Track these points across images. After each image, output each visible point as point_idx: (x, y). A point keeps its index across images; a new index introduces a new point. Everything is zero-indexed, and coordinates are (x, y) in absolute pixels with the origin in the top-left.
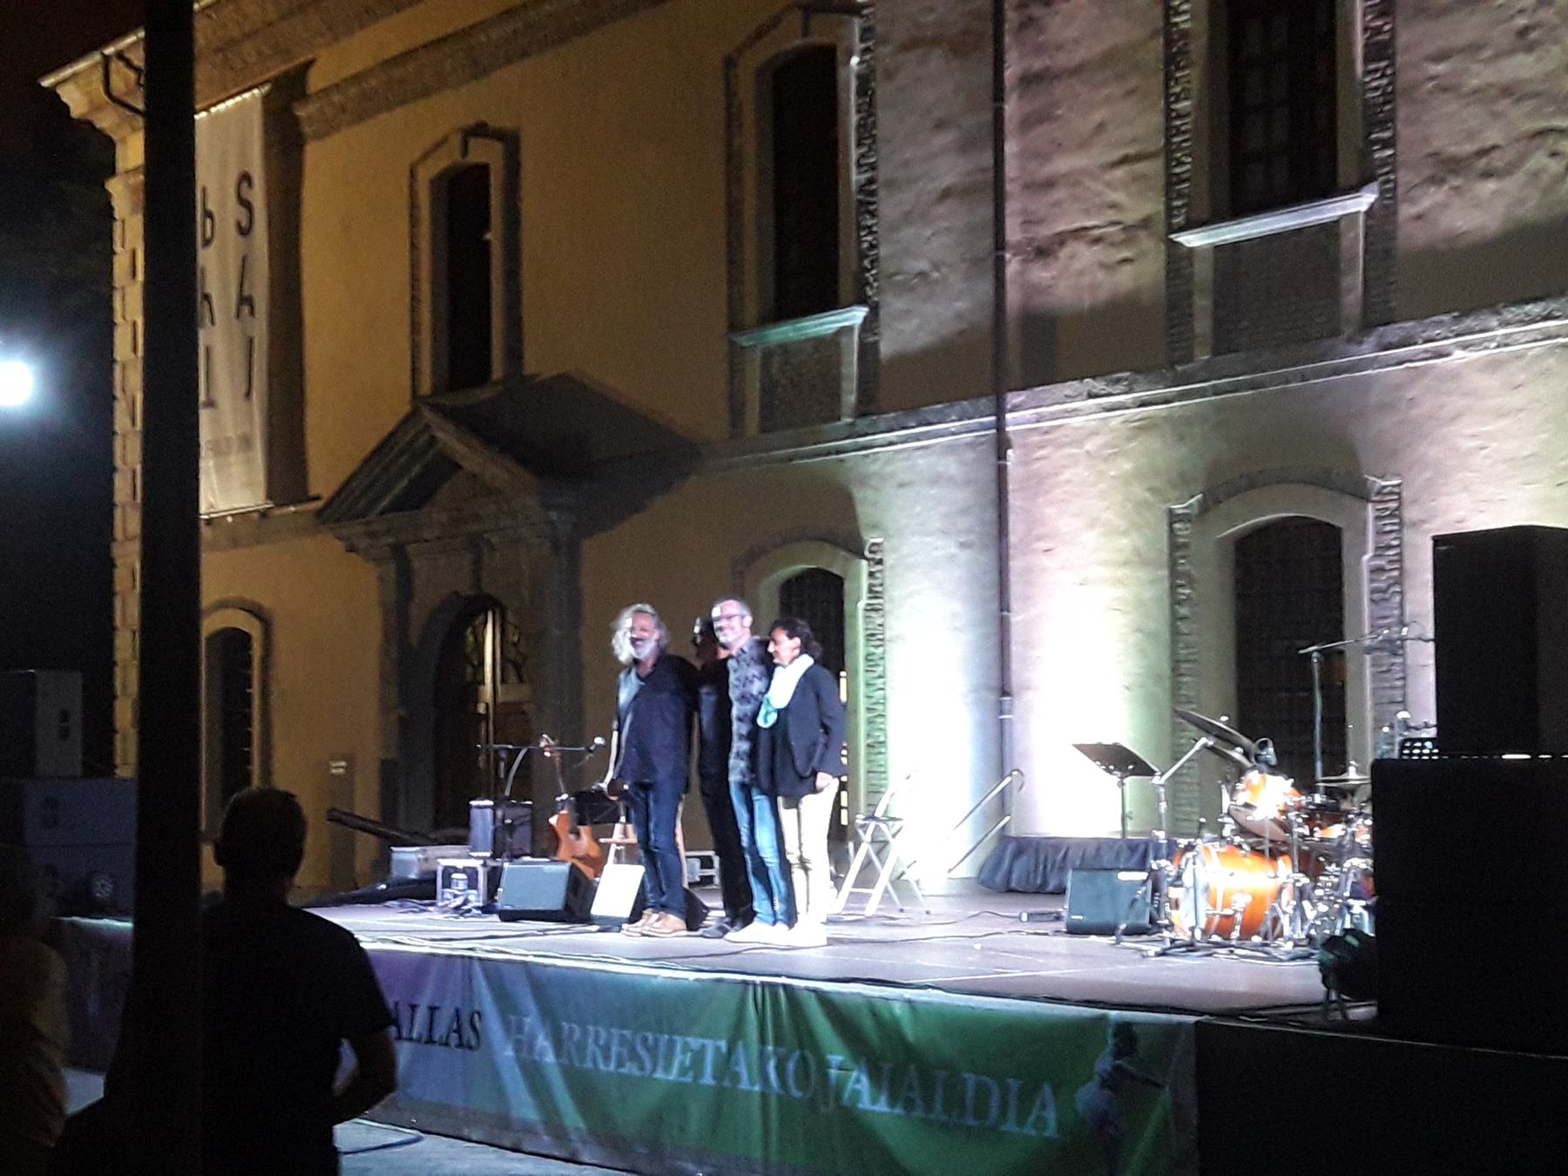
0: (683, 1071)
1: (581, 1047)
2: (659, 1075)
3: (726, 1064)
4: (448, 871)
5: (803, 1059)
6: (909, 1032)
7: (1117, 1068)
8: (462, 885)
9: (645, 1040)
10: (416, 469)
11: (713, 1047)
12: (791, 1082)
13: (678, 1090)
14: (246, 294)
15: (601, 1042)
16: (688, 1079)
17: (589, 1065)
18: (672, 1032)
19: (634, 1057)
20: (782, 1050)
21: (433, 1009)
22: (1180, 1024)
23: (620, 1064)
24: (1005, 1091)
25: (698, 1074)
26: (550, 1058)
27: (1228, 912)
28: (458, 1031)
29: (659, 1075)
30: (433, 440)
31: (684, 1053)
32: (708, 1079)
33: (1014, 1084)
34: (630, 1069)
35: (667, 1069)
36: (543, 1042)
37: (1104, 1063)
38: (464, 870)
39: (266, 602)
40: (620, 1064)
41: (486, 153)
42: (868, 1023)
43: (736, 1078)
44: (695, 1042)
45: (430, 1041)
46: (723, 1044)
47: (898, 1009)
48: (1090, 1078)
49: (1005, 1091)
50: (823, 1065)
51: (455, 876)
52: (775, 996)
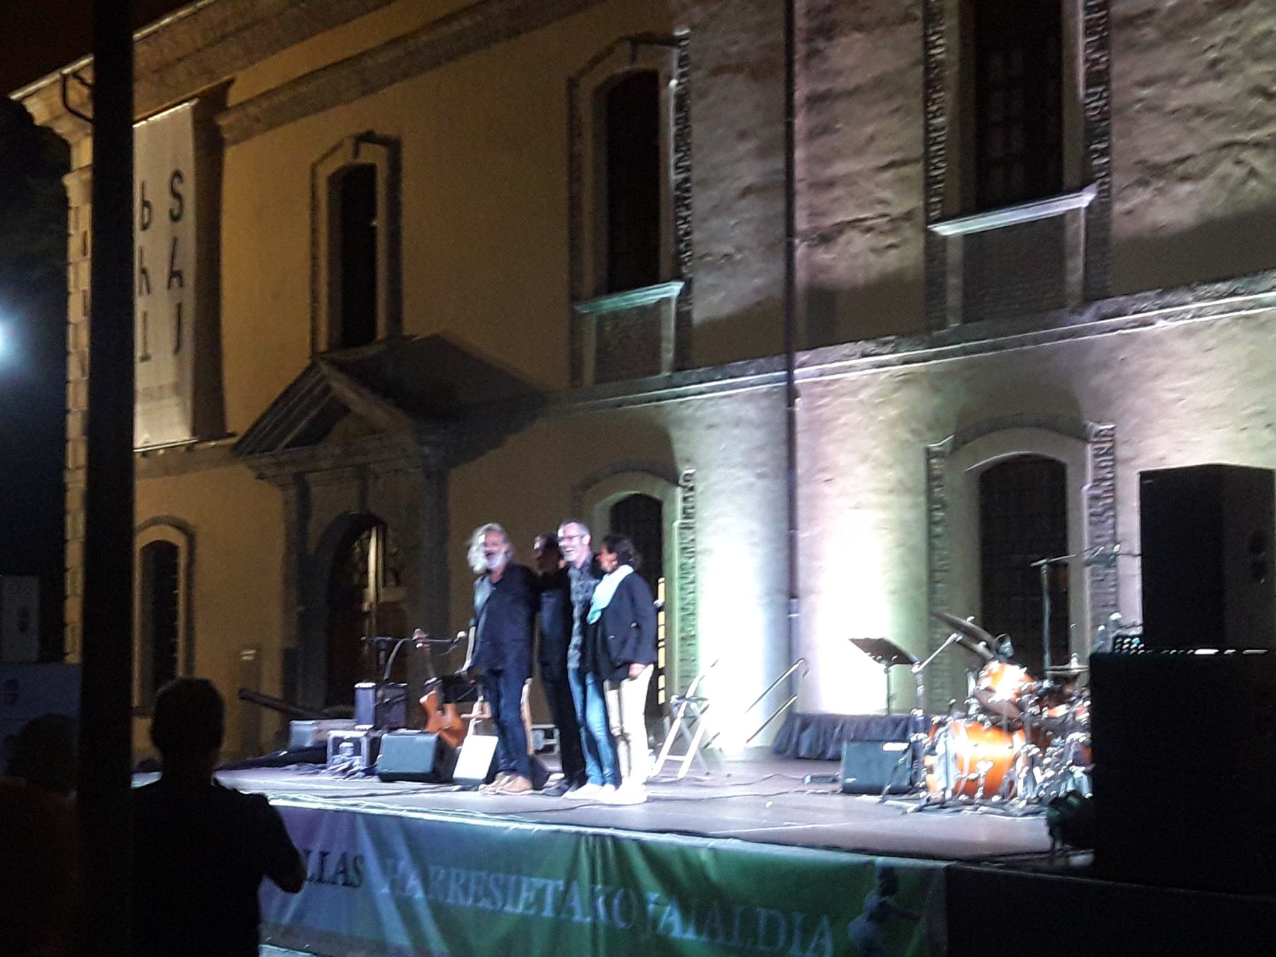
0: (527, 907)
1: (445, 883)
2: (508, 908)
3: (563, 900)
4: (338, 741)
5: (626, 898)
6: (713, 873)
7: (882, 905)
8: (349, 752)
9: (497, 880)
10: (314, 413)
11: (553, 886)
12: (616, 912)
13: (524, 920)
14: (176, 268)
15: (462, 881)
16: (532, 912)
17: (450, 901)
18: (519, 872)
19: (488, 894)
20: (610, 889)
21: (324, 855)
22: (933, 870)
23: (477, 900)
24: (790, 923)
25: (541, 909)
26: (419, 895)
27: (973, 776)
28: (344, 872)
29: (508, 908)
30: (328, 389)
31: (528, 891)
32: (548, 912)
33: (798, 918)
34: (485, 903)
35: (515, 903)
36: (413, 882)
37: (872, 899)
38: (349, 740)
39: (189, 518)
40: (477, 900)
41: (373, 155)
42: (678, 869)
43: (571, 912)
44: (538, 882)
45: (320, 880)
46: (561, 883)
47: (704, 856)
48: (859, 914)
49: (790, 923)
50: (643, 901)
51: (344, 745)
52: (604, 847)
